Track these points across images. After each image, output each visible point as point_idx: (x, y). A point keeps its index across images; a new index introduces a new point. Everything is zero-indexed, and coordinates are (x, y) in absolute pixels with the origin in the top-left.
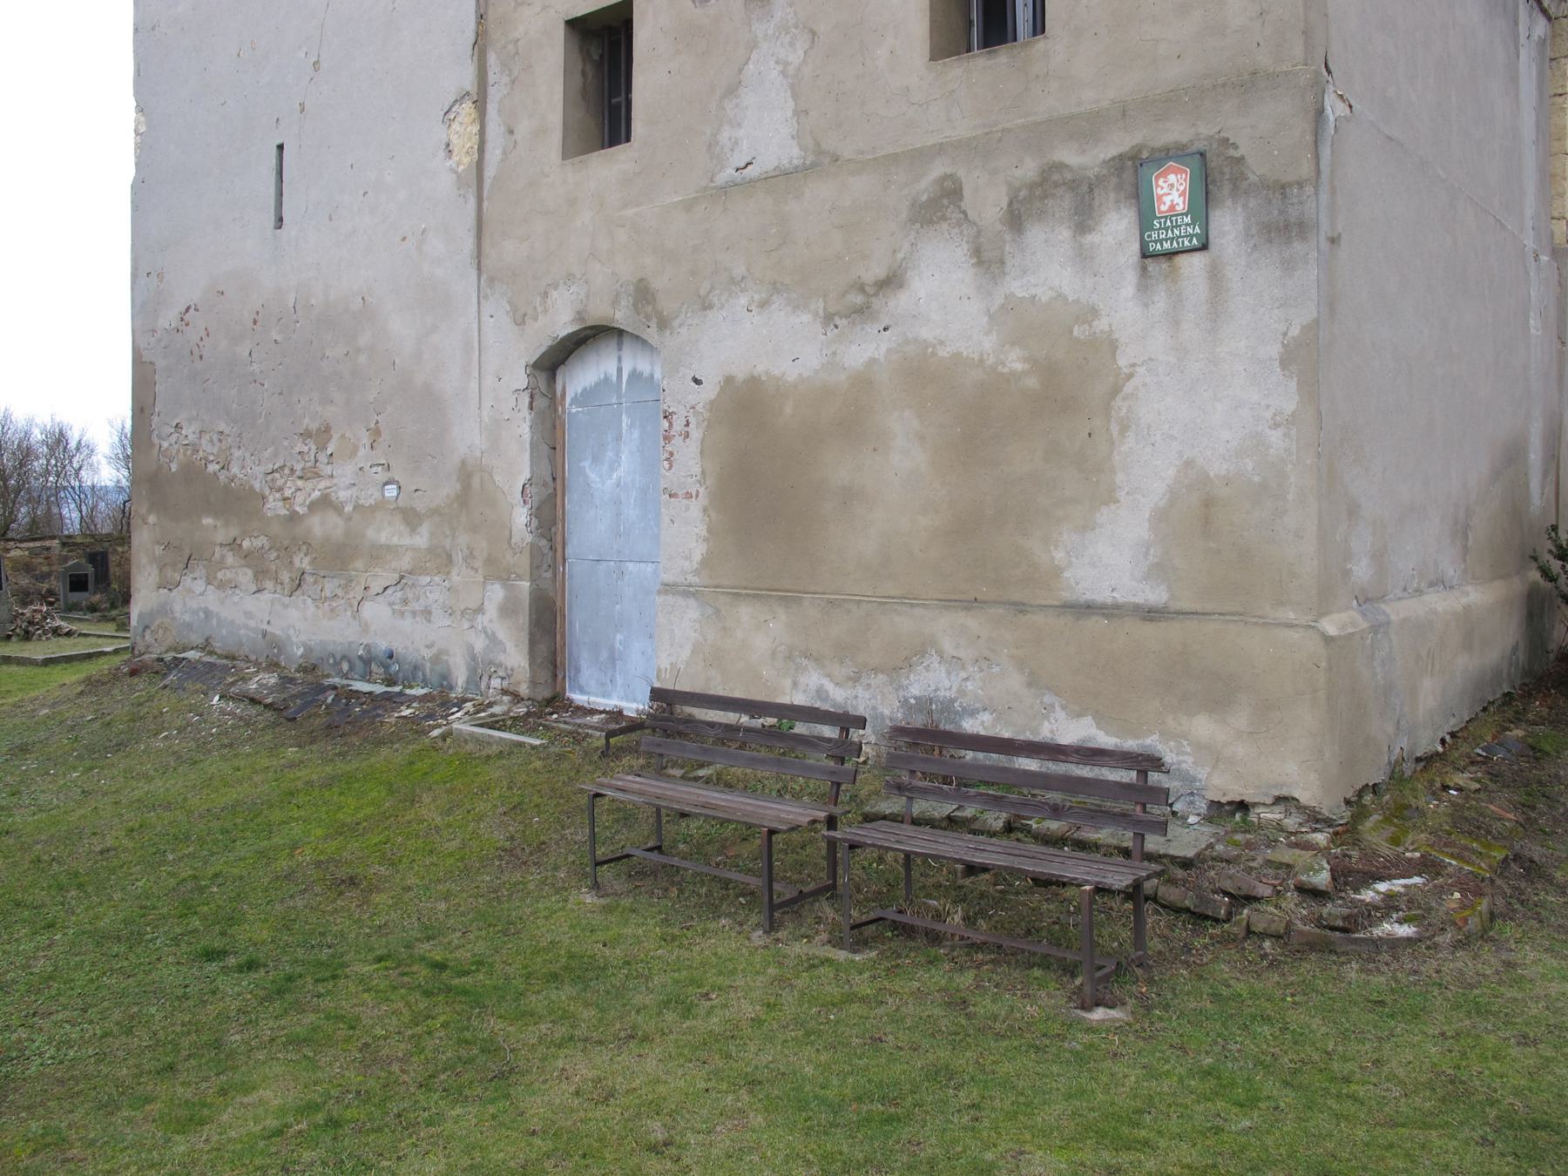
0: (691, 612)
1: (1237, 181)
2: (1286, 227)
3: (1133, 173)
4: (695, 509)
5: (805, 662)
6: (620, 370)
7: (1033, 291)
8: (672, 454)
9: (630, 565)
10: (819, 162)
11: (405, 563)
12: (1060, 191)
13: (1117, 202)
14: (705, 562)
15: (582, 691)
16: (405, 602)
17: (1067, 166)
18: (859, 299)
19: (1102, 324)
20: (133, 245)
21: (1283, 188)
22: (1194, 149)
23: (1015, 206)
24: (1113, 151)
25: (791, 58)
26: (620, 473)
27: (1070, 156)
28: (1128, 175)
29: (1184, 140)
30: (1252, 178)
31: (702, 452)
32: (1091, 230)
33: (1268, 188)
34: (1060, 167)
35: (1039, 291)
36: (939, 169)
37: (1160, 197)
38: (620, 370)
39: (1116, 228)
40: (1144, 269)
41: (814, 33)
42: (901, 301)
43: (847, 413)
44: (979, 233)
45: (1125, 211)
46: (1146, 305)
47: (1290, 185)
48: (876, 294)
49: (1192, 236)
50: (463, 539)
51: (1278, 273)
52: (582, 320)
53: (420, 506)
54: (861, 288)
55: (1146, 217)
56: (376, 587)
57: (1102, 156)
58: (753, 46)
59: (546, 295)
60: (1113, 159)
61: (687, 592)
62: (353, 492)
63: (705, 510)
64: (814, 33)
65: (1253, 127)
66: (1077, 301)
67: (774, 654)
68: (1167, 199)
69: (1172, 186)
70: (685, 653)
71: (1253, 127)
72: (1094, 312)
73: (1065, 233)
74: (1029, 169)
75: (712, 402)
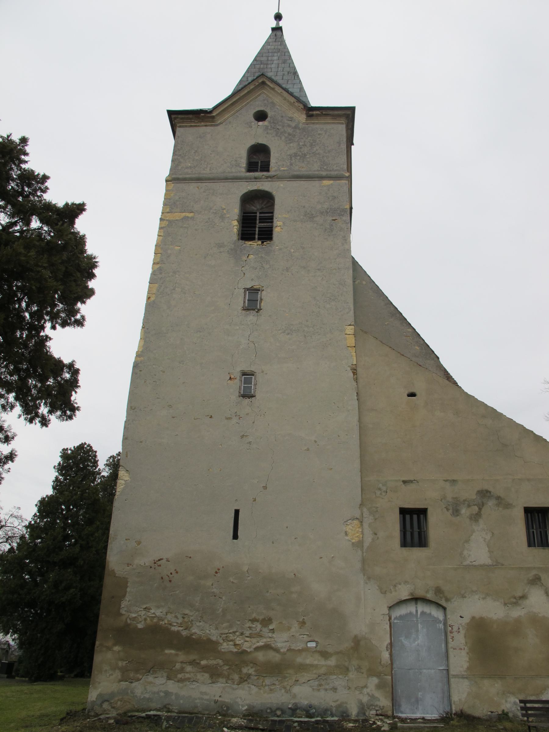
0: (466, 682)
4: (464, 653)
5: (509, 695)
6: (417, 611)
8: (453, 637)
9: (424, 671)
10: (496, 565)
11: (323, 670)
14: (468, 668)
15: (402, 713)
16: (320, 685)
18: (514, 600)
25: (486, 538)
26: (419, 641)
31: (465, 637)
36: (534, 572)
38: (417, 611)
41: (493, 533)
42: (527, 602)
43: (516, 628)
44: (546, 589)
48: (519, 600)
50: (355, 663)
52: (413, 595)
53: (330, 650)
54: (515, 598)
56: (302, 680)
58: (473, 531)
59: (395, 586)
61: (463, 677)
62: (288, 644)
63: (467, 653)
64: (493, 533)
67: (498, 694)
70: (465, 695)
75: (468, 623)
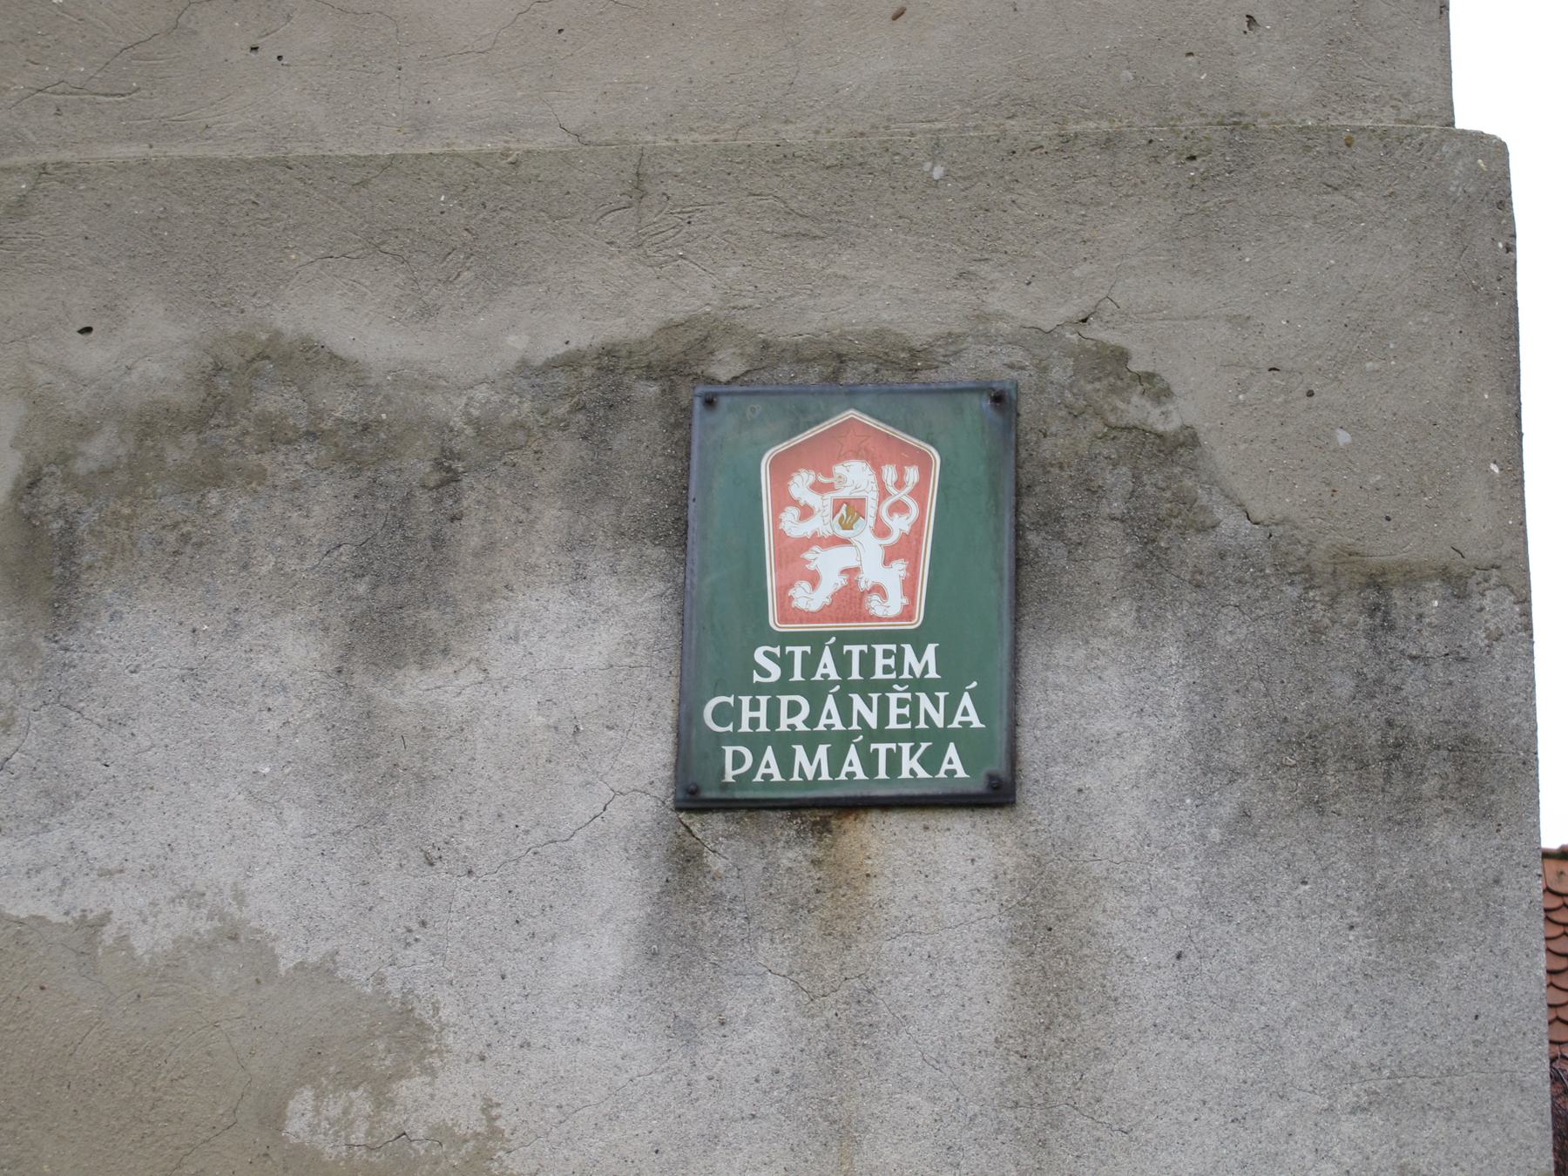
1: (1162, 540)
2: (1395, 750)
3: (665, 444)
7: (89, 897)
12: (286, 465)
13: (574, 544)
17: (338, 362)
19: (443, 1099)
20: (1535, 811)
21: (1377, 585)
22: (962, 371)
23: (53, 496)
24: (571, 331)
27: (359, 323)
28: (637, 441)
29: (920, 327)
30: (1230, 523)
32: (429, 650)
33: (1308, 576)
34: (306, 359)
35: (123, 902)
37: (793, 551)
39: (558, 666)
40: (686, 861)
45: (608, 590)
46: (685, 1032)
47: (1412, 577)
49: (939, 738)
51: (1357, 950)
55: (716, 619)
57: (516, 344)
60: (571, 362)
65: (1239, 322)
66: (324, 972)
68: (830, 565)
69: (852, 509)
71: (1239, 322)
72: (410, 1035)
73: (294, 651)
74: (149, 347)
